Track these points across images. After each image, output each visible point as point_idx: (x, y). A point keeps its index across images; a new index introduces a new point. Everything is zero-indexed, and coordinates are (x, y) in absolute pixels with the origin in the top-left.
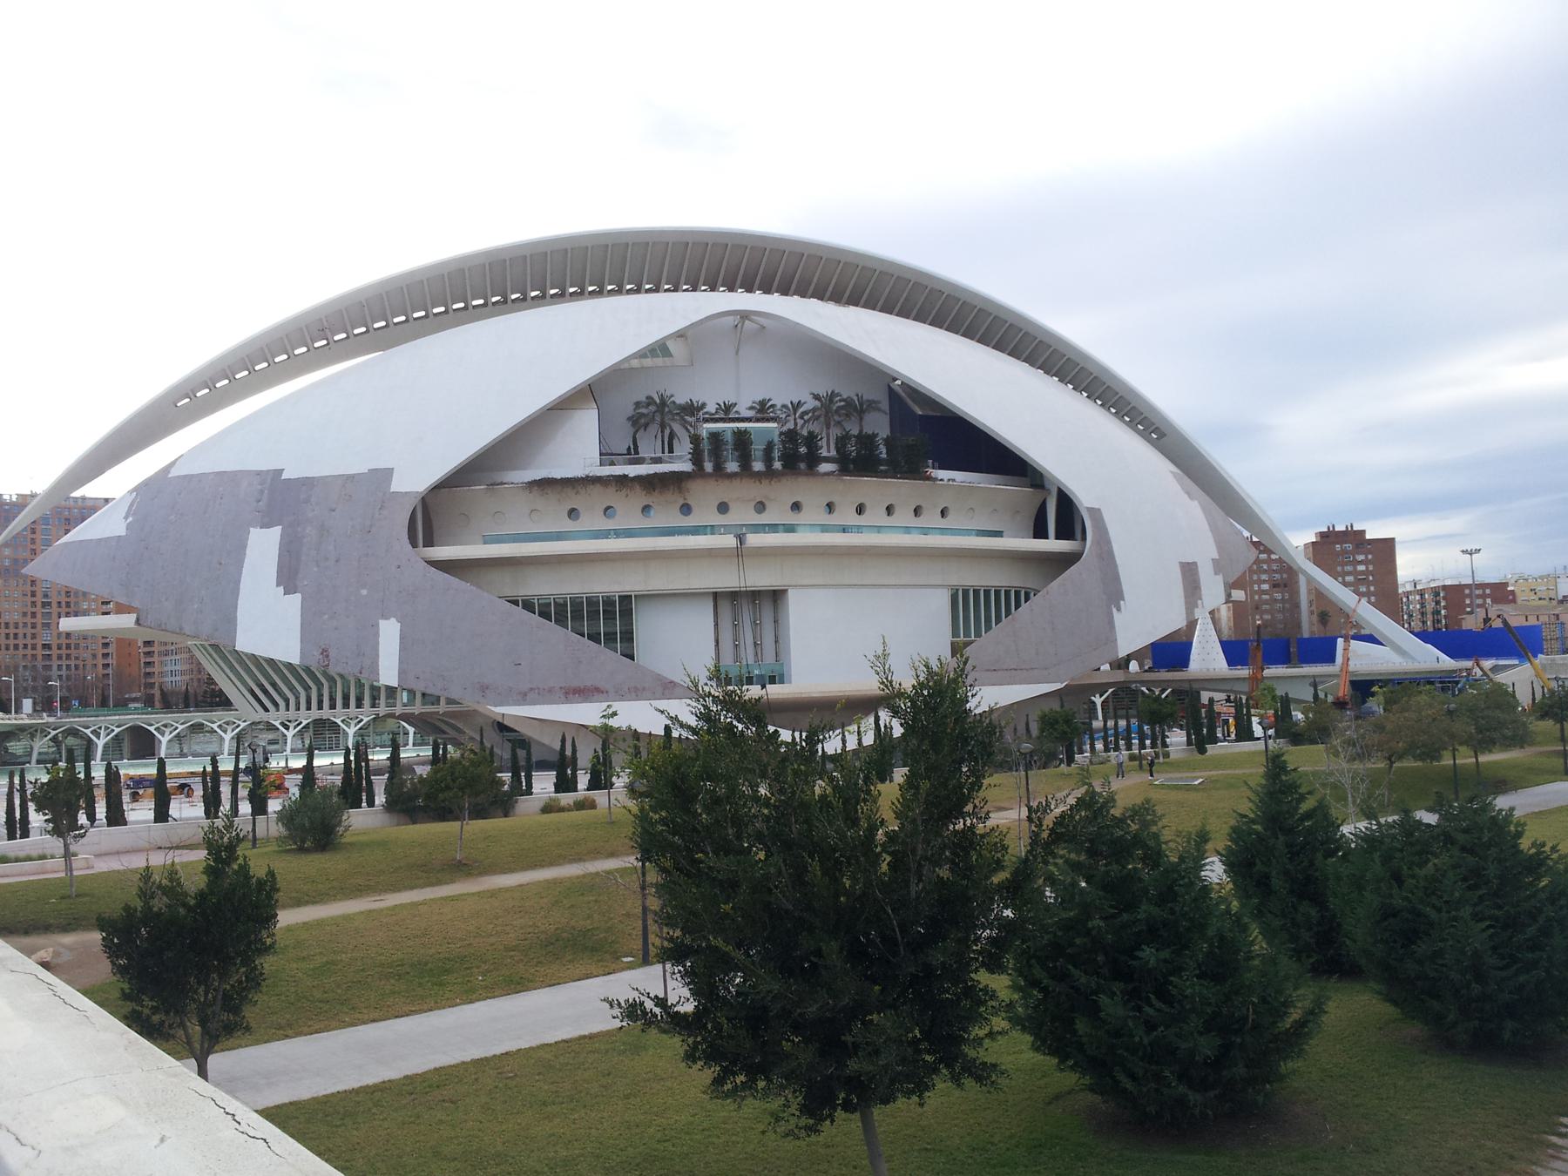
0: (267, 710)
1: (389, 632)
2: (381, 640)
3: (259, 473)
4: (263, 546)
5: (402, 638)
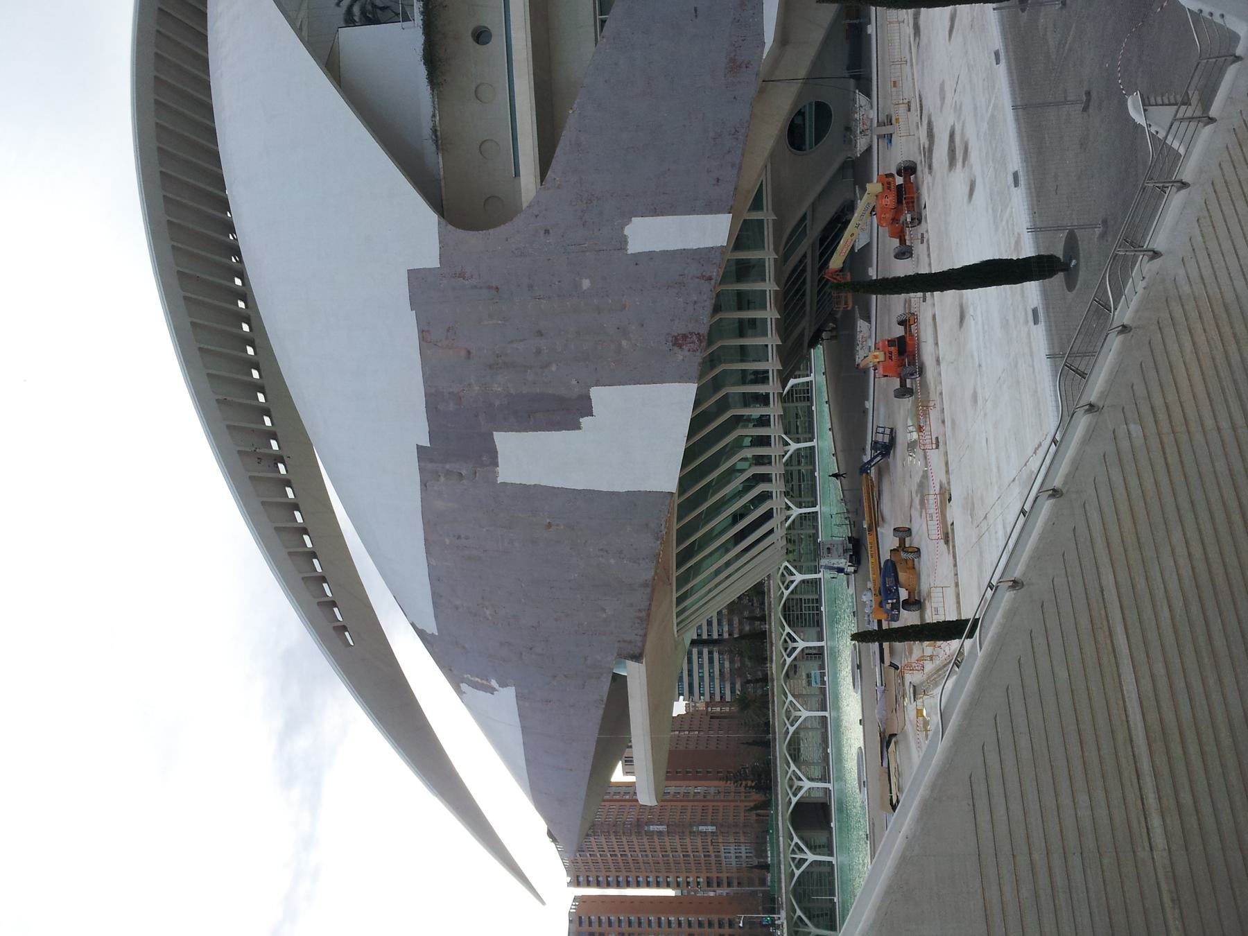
0: (772, 531)
1: (649, 234)
2: (658, 247)
3: (424, 485)
4: (525, 458)
5: (655, 212)
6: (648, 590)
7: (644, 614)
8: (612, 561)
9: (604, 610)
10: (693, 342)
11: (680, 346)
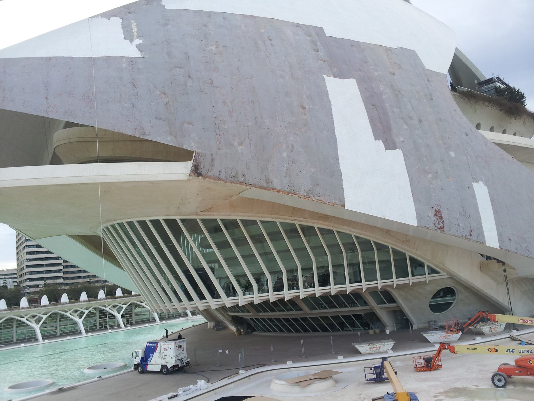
0: (180, 301)
4: (344, 97)
6: (264, 184)
7: (241, 179)
8: (285, 155)
9: (241, 144)
11: (435, 215)
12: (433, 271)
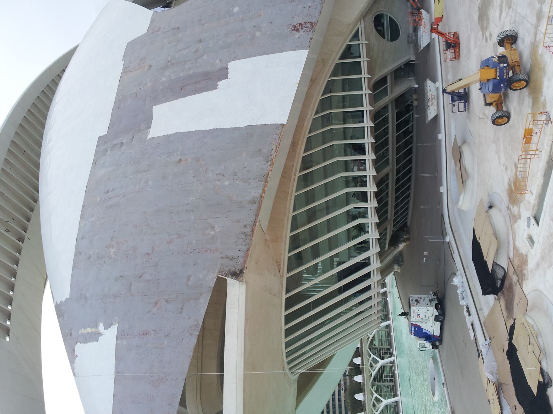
4: (172, 118)
6: (255, 206)
7: (248, 230)
8: (227, 183)
9: (213, 228)
10: (307, 27)
11: (298, 30)
12: (356, 36)
